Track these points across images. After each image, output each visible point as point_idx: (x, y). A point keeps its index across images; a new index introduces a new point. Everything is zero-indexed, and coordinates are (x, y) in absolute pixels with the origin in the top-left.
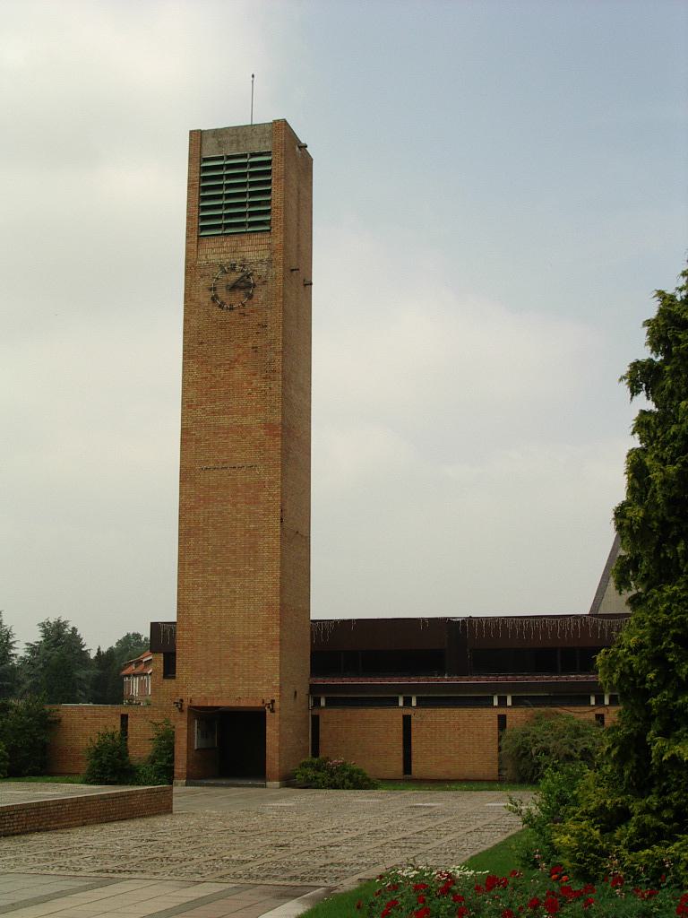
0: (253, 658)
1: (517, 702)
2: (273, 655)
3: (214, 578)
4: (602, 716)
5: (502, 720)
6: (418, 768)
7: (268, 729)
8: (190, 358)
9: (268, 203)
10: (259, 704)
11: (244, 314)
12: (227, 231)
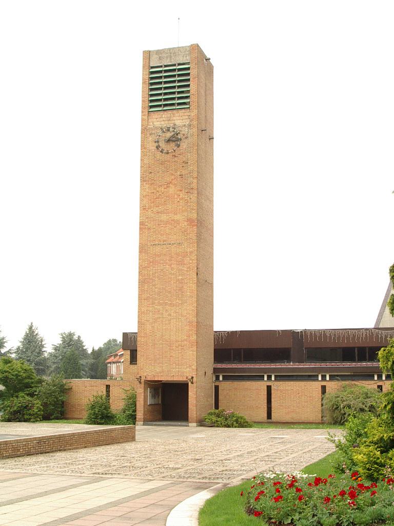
5: (324, 389)
12: (165, 109)
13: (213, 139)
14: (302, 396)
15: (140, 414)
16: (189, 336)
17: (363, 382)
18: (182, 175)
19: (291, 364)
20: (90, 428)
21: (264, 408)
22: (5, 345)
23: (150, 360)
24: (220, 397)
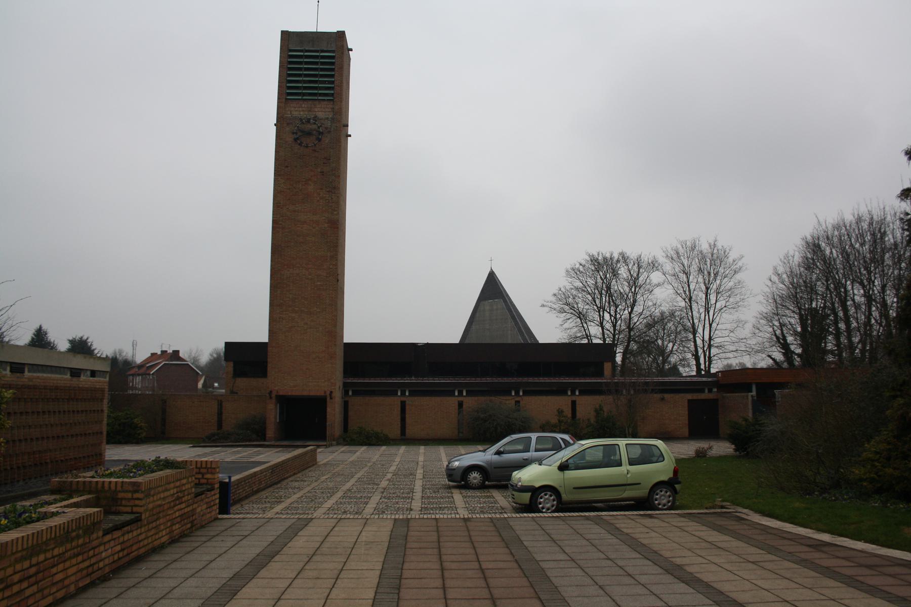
1: (469, 393)
3: (293, 315)
4: (405, 402)
5: (461, 405)
6: (410, 432)
8: (279, 175)
9: (333, 82)
10: (323, 394)
11: (315, 151)
12: (304, 98)
13: (348, 126)
17: (502, 397)
18: (323, 172)
19: (413, 378)
20: (205, 455)
24: (350, 413)
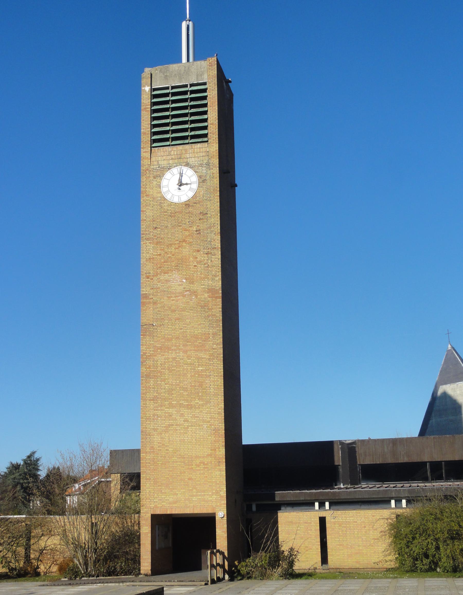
0: (204, 474)
2: (220, 470)
3: (170, 410)
7: (218, 531)
14: (369, 530)
15: (146, 564)
16: (215, 450)
21: (317, 549)
22: (40, 463)
23: (159, 486)
